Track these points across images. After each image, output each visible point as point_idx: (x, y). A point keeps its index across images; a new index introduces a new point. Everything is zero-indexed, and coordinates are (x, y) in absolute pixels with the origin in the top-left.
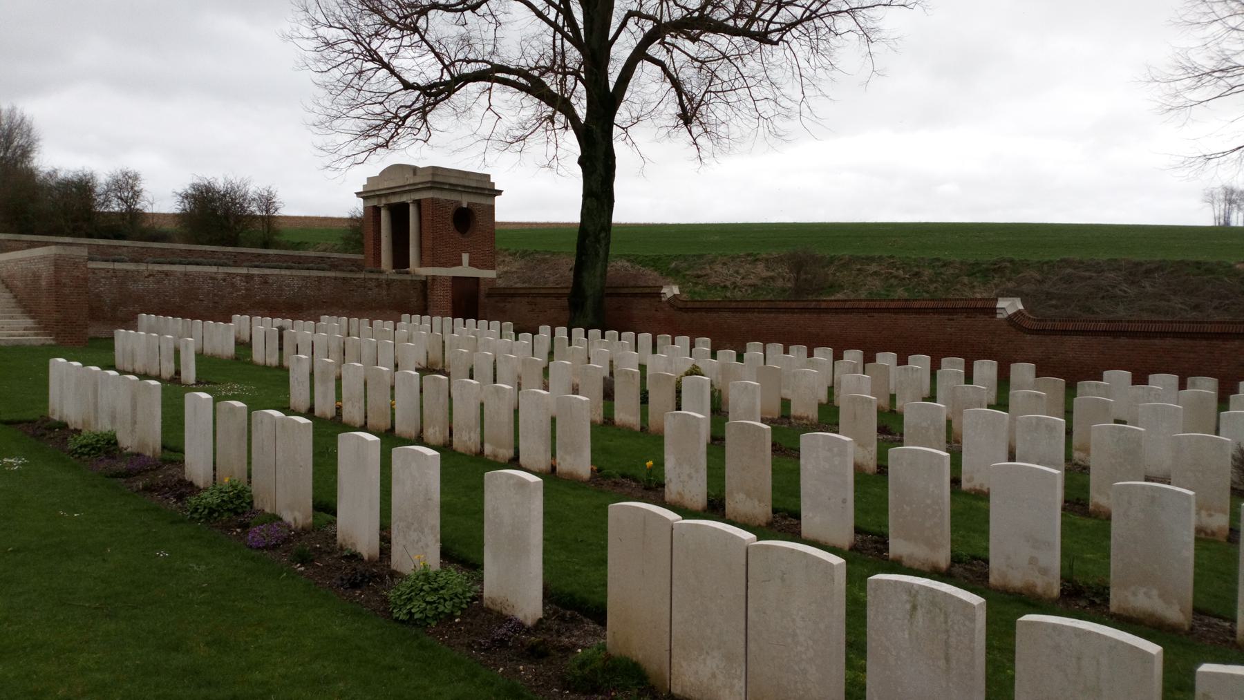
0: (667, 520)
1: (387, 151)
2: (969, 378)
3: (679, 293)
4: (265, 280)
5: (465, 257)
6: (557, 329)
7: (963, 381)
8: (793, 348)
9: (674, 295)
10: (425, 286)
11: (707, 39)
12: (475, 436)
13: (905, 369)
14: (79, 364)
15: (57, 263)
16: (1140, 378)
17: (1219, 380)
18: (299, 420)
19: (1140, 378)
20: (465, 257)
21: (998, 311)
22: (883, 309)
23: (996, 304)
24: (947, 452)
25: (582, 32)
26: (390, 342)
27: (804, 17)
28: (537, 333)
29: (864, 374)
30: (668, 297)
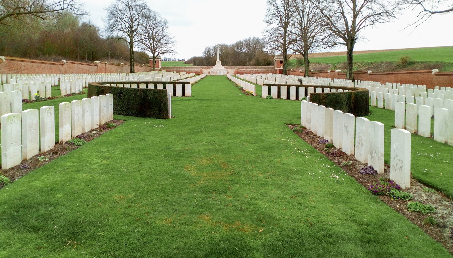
5: (281, 66)
20: (281, 66)
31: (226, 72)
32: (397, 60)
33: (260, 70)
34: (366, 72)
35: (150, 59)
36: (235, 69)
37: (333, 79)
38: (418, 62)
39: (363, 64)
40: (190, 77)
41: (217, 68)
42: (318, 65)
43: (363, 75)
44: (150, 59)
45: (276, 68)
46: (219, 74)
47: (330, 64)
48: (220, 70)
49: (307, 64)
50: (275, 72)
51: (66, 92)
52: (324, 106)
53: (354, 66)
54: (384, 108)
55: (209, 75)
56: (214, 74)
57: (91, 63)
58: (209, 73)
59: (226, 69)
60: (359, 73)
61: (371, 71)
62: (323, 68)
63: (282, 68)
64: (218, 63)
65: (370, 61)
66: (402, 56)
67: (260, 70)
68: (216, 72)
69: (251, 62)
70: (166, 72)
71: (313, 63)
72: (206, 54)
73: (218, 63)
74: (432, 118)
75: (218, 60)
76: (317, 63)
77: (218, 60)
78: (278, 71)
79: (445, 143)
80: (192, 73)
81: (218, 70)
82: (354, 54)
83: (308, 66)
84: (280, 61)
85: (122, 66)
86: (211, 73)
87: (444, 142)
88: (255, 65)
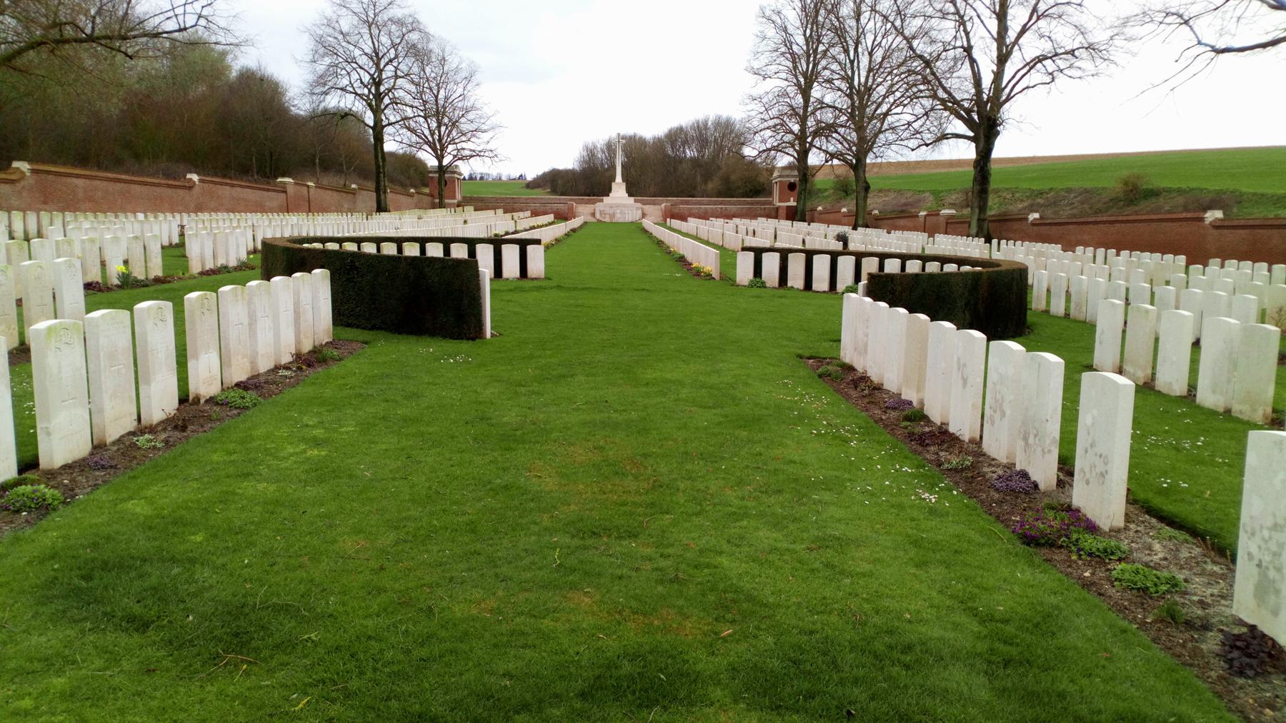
0: (1115, 382)
10: (777, 209)
15: (665, 206)
20: (792, 199)
31: (640, 212)
32: (1111, 184)
33: (733, 208)
35: (431, 175)
36: (665, 203)
37: (931, 235)
38: (1169, 191)
40: (541, 226)
41: (614, 202)
42: (892, 195)
43: (1016, 225)
44: (431, 175)
45: (779, 204)
46: (619, 218)
48: (625, 206)
49: (862, 194)
50: (774, 214)
53: (992, 201)
55: (594, 220)
56: (607, 220)
57: (268, 183)
58: (593, 215)
59: (639, 205)
62: (906, 205)
63: (792, 203)
64: (619, 190)
66: (1125, 173)
67: (733, 208)
68: (611, 212)
69: (710, 186)
70: (475, 210)
71: (880, 191)
72: (584, 161)
73: (619, 190)
74: (1196, 344)
75: (619, 178)
77: (619, 178)
78: (782, 213)
80: (545, 213)
81: (618, 206)
83: (865, 198)
84: (787, 183)
85: (353, 193)
86: (598, 216)
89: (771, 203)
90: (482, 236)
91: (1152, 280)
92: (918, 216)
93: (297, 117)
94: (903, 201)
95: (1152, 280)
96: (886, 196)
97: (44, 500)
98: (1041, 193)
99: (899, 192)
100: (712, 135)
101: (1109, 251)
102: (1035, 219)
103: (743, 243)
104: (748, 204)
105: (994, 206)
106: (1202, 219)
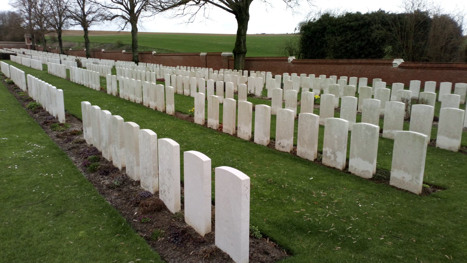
1: (305, 16)
2: (453, 91)
3: (246, 56)
4: (9, 45)
6: (427, 83)
7: (403, 88)
8: (202, 68)
9: (293, 59)
10: (27, 46)
11: (175, 9)
12: (291, 142)
13: (397, 85)
14: (122, 118)
16: (317, 76)
17: (421, 82)
18: (147, 131)
19: (317, 76)
21: (393, 64)
22: (406, 67)
23: (392, 61)
24: (234, 99)
25: (227, 3)
26: (188, 77)
27: (139, 9)
28: (176, 67)
29: (337, 83)
30: (399, 65)
32: (114, 42)
34: (284, 59)
37: (116, 61)
38: (126, 44)
39: (98, 44)
42: (68, 43)
45: (27, 44)
47: (77, 43)
49: (44, 43)
50: (26, 47)
51: (434, 13)
52: (99, 106)
53: (64, 44)
54: (318, 160)
60: (94, 51)
61: (155, 52)
62: (70, 46)
63: (31, 44)
65: (102, 42)
76: (67, 41)
78: (29, 47)
79: (101, 90)
82: (89, 35)
83: (45, 44)
87: (231, 134)
88: (28, 99)
89: (25, 44)
90: (166, 87)
91: (382, 118)
92: (84, 50)
93: (462, 35)
94: (70, 44)
95: (382, 118)
96: (66, 43)
97: (419, 22)
98: (103, 44)
99: (70, 42)
100: (136, 33)
101: (244, 71)
102: (155, 53)
103: (156, 78)
104: (17, 44)
105: (91, 46)
106: (122, 52)
